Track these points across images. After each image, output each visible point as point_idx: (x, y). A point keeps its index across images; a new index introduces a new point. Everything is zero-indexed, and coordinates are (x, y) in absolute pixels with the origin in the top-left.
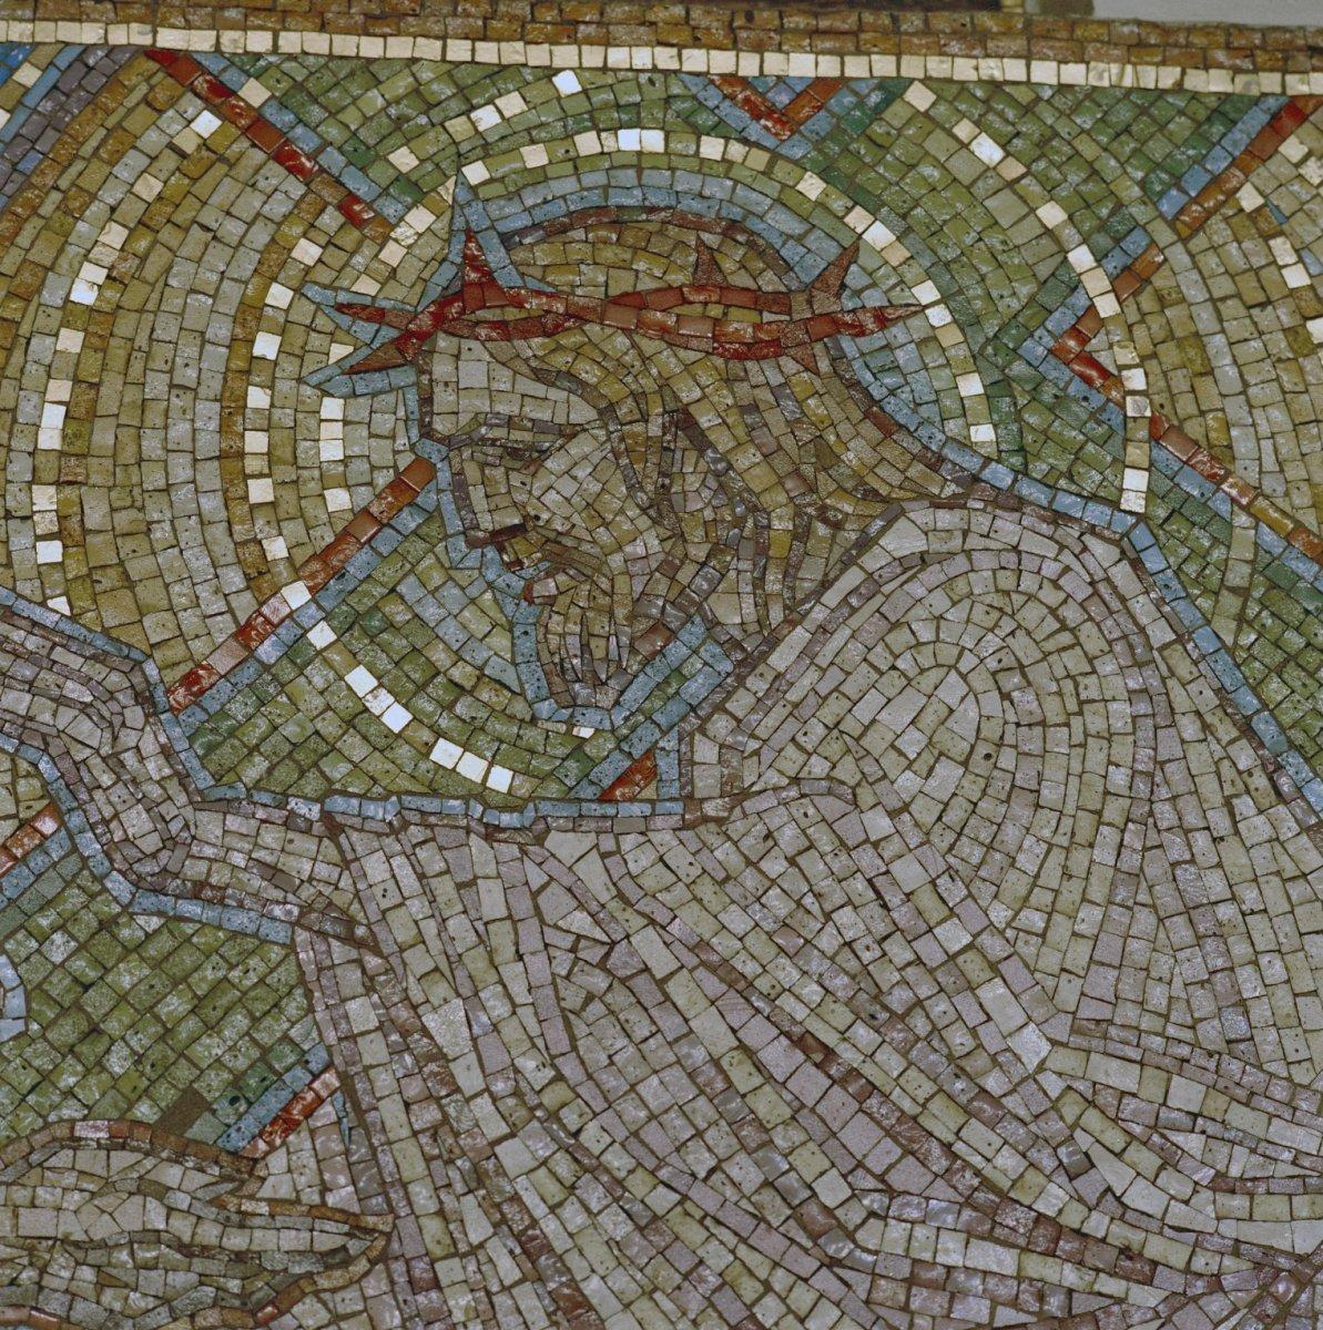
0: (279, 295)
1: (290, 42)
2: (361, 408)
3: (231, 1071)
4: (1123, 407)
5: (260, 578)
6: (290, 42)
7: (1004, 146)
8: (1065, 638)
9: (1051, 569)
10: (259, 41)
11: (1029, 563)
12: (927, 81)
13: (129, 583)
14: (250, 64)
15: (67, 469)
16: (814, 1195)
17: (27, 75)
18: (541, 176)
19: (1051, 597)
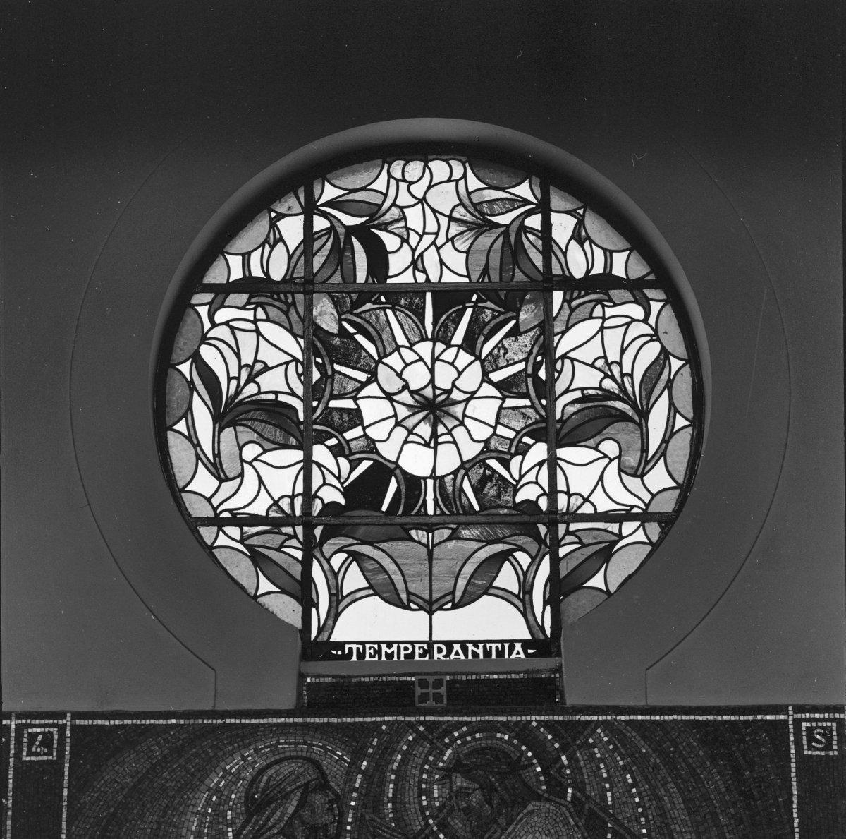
0: (427, 767)
1: (427, 718)
2: (440, 787)
3: (644, 518)
4: (672, 778)
5: (425, 818)
6: (427, 718)
7: (438, 828)
8: (556, 825)
9: (555, 812)
10: (422, 719)
11: (551, 811)
12: (536, 721)
13: (404, 820)
14: (421, 723)
15: (393, 800)
16: (404, 218)
17: (384, 727)
18: (470, 742)
19: (555, 817)
